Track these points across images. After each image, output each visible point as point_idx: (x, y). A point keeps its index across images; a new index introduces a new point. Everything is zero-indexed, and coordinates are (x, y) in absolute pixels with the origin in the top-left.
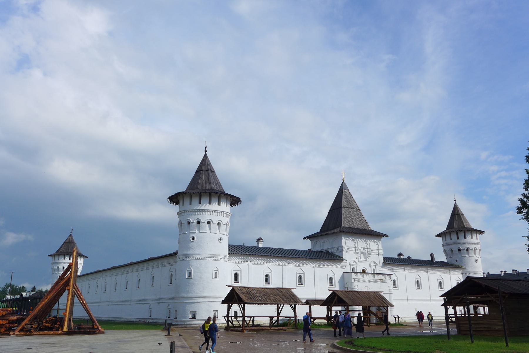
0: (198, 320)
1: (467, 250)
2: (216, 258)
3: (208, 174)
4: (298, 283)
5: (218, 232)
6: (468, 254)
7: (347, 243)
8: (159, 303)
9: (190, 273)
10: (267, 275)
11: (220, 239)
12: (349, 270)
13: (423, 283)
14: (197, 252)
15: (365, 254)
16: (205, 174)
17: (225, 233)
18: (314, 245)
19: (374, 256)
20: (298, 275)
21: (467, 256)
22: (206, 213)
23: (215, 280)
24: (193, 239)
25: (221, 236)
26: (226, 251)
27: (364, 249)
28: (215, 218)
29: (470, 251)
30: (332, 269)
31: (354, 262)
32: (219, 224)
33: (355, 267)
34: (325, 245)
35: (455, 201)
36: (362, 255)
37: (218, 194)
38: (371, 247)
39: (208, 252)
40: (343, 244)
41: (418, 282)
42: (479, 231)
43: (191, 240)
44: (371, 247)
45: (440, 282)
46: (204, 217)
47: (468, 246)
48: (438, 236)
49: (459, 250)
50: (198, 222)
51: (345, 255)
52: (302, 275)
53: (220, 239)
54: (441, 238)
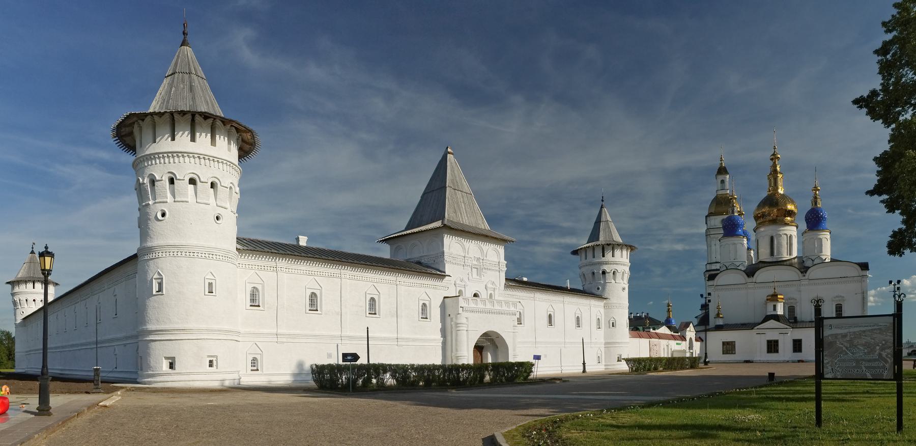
0: (180, 374)
2: (210, 254)
3: (190, 77)
4: (308, 308)
5: (212, 200)
6: (605, 279)
7: (452, 245)
8: (125, 345)
9: (160, 285)
11: (218, 218)
13: (326, 302)
14: (171, 242)
15: (480, 270)
17: (228, 205)
18: (394, 252)
20: (369, 297)
21: (613, 281)
22: (187, 159)
23: (210, 297)
24: (163, 215)
25: (220, 211)
26: (233, 245)
27: (478, 259)
28: (206, 174)
29: (618, 274)
30: (428, 290)
32: (213, 185)
33: (463, 289)
34: (417, 251)
36: (475, 270)
37: (210, 121)
39: (193, 242)
41: (550, 316)
45: (578, 318)
46: (184, 169)
47: (614, 267)
49: (604, 273)
50: (172, 181)
51: (448, 269)
52: (376, 297)
53: (218, 218)
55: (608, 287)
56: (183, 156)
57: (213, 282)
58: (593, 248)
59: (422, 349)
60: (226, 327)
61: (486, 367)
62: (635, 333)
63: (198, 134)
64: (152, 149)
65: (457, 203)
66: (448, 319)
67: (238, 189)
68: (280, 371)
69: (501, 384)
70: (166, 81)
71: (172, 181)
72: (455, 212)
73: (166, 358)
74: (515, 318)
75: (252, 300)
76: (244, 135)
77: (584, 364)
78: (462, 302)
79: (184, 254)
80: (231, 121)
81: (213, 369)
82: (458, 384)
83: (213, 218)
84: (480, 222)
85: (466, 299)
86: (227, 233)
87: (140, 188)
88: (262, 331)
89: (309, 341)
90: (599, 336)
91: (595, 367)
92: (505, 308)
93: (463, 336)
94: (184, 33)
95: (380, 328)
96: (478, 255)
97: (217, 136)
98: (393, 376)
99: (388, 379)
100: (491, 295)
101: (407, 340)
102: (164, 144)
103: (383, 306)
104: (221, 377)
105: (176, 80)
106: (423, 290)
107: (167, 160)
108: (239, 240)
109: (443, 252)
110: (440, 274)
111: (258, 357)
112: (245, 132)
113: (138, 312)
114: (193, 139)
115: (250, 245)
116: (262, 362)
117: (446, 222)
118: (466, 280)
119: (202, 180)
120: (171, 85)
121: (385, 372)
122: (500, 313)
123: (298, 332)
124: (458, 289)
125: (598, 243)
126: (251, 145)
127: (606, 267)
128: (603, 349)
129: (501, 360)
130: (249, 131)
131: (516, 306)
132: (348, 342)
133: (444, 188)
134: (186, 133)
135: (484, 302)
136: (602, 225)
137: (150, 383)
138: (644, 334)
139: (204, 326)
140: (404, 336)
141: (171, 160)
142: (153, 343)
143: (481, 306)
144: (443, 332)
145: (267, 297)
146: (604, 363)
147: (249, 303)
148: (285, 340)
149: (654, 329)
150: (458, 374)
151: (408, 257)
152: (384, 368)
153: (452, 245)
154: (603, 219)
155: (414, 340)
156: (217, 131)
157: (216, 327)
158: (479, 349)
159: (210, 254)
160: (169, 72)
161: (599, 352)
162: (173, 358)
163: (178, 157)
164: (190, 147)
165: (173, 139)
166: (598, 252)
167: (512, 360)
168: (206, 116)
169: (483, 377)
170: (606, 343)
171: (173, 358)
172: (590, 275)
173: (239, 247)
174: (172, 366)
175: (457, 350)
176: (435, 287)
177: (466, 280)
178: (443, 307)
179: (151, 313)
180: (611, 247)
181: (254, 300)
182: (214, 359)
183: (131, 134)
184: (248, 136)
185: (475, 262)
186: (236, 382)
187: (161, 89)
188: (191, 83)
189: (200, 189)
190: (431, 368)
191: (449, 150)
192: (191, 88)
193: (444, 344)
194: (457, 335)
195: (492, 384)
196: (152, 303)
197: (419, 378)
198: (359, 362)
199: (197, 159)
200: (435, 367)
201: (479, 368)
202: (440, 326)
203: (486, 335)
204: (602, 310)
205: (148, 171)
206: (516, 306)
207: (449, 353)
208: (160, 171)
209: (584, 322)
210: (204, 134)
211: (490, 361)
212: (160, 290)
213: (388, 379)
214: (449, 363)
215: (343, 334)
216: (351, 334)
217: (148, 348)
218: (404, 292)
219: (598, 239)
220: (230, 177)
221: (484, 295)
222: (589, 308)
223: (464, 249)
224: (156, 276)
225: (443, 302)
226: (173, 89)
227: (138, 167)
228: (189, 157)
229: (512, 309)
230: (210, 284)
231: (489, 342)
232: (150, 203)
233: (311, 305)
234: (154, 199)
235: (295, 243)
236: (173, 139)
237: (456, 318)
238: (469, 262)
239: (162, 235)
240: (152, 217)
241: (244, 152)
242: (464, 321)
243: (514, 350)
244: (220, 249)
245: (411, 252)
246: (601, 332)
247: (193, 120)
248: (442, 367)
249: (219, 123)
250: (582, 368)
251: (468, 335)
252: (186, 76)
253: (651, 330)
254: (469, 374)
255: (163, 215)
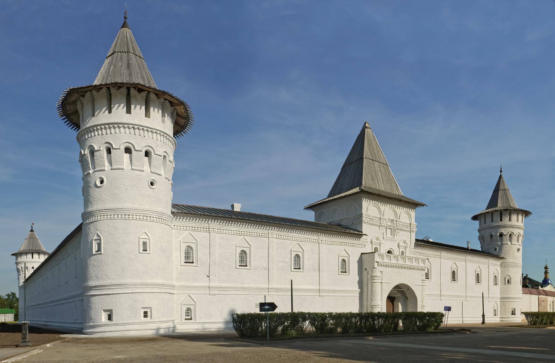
0: (117, 324)
1: (510, 235)
2: (145, 216)
3: (128, 55)
4: (238, 264)
5: (146, 168)
6: (502, 241)
7: (369, 208)
9: (99, 245)
10: (243, 252)
11: (152, 184)
12: (369, 249)
14: (108, 206)
16: (121, 58)
17: (162, 172)
19: (405, 233)
20: (294, 254)
21: (509, 243)
22: (122, 130)
23: (145, 255)
24: (102, 182)
25: (154, 177)
26: (168, 210)
27: (392, 221)
28: (140, 143)
31: (377, 239)
33: (378, 247)
34: (338, 214)
35: (501, 171)
36: (389, 231)
37: (144, 94)
38: (401, 220)
39: (129, 205)
40: (364, 211)
41: (454, 273)
42: (522, 211)
43: (98, 183)
44: (401, 220)
45: (478, 275)
47: (512, 230)
48: (475, 218)
49: (501, 235)
51: (365, 229)
53: (152, 184)
54: (477, 223)
55: (505, 248)
56: (119, 127)
57: (148, 241)
58: (492, 213)
59: (343, 300)
60: (160, 281)
61: (398, 316)
62: (527, 289)
63: (133, 107)
64: (92, 122)
65: (375, 172)
66: (365, 273)
67: (172, 158)
68: (214, 320)
69: (414, 333)
70: (107, 61)
71: (109, 151)
72: (373, 180)
73: (105, 311)
74: (424, 273)
75: (187, 257)
76: (178, 108)
77: (483, 316)
78: (377, 258)
79: (120, 216)
80: (164, 93)
81: (148, 319)
82: (373, 331)
83: (147, 184)
84: (395, 189)
85: (381, 256)
86: (163, 197)
87: (82, 158)
88: (195, 284)
89: (239, 293)
90: (496, 291)
91: (492, 320)
92: (415, 264)
93: (378, 287)
94: (125, 18)
95: (303, 281)
96: (392, 217)
97: (152, 109)
98: (312, 324)
99: (307, 325)
100: (403, 252)
101: (329, 291)
102: (102, 117)
103: (307, 261)
104: (155, 326)
105: (115, 59)
106: (343, 247)
107: (104, 131)
108: (174, 206)
109: (361, 215)
110: (358, 234)
111: (192, 307)
112: (178, 105)
113: (82, 273)
114: (129, 111)
115: (182, 210)
116: (195, 312)
117: (363, 188)
118: (381, 239)
119: (137, 148)
120: (110, 64)
121: (304, 320)
122: (410, 268)
123: (229, 285)
124: (374, 246)
125: (497, 209)
126: (185, 118)
127: (503, 231)
128: (499, 303)
129: (410, 310)
130: (182, 103)
131: (424, 263)
132: (275, 293)
133: (362, 159)
134: (122, 105)
135: (396, 258)
136: (500, 193)
137: (91, 333)
138: (534, 290)
139: (138, 281)
140: (325, 288)
141: (108, 131)
142: (93, 298)
143: (394, 261)
144: (361, 284)
145: (200, 255)
146: (499, 316)
147: (183, 260)
148: (216, 292)
149: (542, 287)
150: (373, 321)
151: (330, 221)
152: (304, 316)
153: (369, 208)
154: (501, 187)
155: (334, 291)
156: (151, 104)
157: (150, 281)
158: (391, 299)
159: (145, 216)
160: (110, 53)
161: (496, 306)
162: (111, 311)
163: (114, 128)
164: (126, 118)
165: (110, 112)
166: (497, 217)
167: (419, 310)
168: (140, 89)
169: (398, 324)
170: (501, 298)
171: (111, 311)
172: (489, 237)
173: (174, 210)
174: (110, 318)
175: (372, 300)
176: (353, 245)
177: (381, 239)
178: (360, 262)
179: (92, 271)
180: (508, 212)
181: (189, 259)
182: (149, 310)
183: (76, 112)
184: (181, 109)
185: (390, 224)
186: (171, 329)
187: (102, 69)
188: (128, 61)
189: (136, 158)
190: (349, 317)
191: (367, 125)
192: (129, 66)
193: (361, 294)
194: (372, 286)
195: (406, 332)
196: (93, 261)
197: (336, 325)
198: (277, 311)
199: (132, 130)
200: (352, 315)
201: (390, 317)
202: (357, 279)
203: (397, 287)
204: (499, 269)
205: (88, 144)
206: (424, 263)
207: (365, 303)
208: (98, 142)
209: (483, 278)
210: (138, 107)
211: (400, 310)
212: (99, 249)
213: (307, 325)
214: (365, 311)
215: (270, 286)
216: (278, 286)
217: (89, 302)
218: (327, 251)
219: (496, 206)
220: (164, 147)
221: (396, 252)
222: (489, 267)
223: (380, 211)
224: (96, 237)
225: (361, 258)
226: (112, 67)
227: (81, 140)
228: (124, 128)
229: (421, 265)
230: (145, 244)
231: (401, 293)
232: (91, 172)
233: (241, 261)
234: (94, 168)
235: (230, 209)
236: (110, 112)
237: (372, 272)
238: (384, 223)
239: (102, 200)
240: (92, 185)
241: (180, 127)
242: (379, 274)
243: (422, 302)
244: (154, 212)
245: (335, 216)
246: (497, 289)
247: (128, 94)
248: (359, 315)
249: (152, 96)
250: (481, 319)
251: (382, 286)
252: (125, 55)
253: (540, 287)
254: (384, 323)
255: (102, 182)
